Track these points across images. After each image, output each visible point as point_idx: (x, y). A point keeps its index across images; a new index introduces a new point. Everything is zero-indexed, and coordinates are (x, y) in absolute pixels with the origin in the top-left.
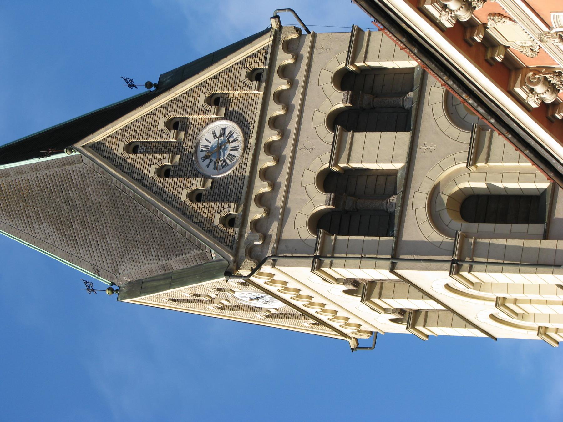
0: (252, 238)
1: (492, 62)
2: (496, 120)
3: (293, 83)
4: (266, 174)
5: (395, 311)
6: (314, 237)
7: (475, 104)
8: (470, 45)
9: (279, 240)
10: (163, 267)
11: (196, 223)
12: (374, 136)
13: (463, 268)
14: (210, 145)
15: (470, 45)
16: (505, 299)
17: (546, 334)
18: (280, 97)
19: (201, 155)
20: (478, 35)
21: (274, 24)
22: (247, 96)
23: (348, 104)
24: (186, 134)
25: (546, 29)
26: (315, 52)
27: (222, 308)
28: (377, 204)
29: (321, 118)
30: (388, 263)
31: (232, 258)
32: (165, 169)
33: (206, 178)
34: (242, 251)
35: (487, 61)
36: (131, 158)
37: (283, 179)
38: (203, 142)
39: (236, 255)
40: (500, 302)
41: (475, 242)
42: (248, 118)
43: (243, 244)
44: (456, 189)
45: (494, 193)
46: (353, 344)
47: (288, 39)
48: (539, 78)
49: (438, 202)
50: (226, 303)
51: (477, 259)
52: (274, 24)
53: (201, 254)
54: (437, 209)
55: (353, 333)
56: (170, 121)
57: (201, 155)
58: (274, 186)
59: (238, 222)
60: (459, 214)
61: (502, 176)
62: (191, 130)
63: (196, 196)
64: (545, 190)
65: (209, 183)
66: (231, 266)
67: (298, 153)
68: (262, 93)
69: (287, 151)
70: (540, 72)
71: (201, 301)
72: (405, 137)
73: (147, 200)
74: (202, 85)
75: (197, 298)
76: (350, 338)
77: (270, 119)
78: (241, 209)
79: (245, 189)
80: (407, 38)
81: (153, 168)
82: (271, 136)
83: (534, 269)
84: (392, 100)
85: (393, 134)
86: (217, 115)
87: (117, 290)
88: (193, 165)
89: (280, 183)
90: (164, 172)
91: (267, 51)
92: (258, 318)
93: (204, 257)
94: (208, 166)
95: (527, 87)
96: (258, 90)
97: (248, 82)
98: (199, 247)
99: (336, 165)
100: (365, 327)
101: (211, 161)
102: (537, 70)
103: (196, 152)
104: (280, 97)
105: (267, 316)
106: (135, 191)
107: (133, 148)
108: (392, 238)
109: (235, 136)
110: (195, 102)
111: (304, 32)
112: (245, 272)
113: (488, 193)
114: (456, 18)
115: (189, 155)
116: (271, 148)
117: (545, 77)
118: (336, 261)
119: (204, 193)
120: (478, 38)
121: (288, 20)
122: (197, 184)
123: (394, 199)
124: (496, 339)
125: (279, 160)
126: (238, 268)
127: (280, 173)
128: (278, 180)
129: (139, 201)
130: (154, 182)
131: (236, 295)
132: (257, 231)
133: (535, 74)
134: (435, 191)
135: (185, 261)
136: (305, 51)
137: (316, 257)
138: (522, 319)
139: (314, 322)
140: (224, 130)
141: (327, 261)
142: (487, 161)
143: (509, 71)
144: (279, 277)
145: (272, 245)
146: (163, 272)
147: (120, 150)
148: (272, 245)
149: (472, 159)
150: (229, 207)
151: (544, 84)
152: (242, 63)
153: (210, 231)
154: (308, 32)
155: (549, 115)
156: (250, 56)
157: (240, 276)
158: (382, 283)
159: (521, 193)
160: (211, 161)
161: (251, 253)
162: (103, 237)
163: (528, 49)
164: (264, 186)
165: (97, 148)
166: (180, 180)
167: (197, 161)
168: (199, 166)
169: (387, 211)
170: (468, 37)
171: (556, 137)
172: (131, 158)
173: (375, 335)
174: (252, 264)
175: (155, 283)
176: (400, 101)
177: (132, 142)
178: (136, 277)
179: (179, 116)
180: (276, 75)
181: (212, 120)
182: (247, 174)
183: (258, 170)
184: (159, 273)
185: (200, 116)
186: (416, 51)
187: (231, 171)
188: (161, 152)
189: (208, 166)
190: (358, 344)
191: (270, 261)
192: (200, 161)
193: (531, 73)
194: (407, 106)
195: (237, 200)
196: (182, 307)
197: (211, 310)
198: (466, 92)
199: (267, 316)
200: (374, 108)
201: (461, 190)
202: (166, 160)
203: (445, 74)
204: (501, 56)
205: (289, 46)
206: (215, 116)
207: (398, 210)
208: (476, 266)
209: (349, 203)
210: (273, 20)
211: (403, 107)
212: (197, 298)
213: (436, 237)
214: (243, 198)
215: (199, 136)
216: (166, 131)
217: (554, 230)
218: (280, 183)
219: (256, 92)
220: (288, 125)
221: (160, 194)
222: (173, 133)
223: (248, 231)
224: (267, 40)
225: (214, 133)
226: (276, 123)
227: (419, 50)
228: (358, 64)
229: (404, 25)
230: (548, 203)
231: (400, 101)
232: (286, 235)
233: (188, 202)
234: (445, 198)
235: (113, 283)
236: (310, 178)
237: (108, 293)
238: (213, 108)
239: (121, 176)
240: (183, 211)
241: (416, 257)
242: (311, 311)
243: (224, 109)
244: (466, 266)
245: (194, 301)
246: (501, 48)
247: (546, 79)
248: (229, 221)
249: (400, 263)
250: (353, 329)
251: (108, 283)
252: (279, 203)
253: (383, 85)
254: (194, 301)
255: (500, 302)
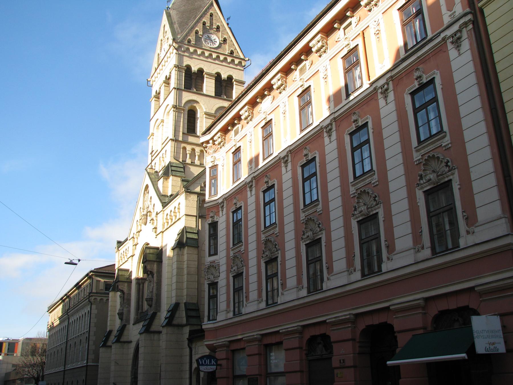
0: (184, 48)
1: (257, 98)
2: (236, 101)
3: (229, 63)
4: (203, 53)
5: (160, 92)
6: (184, 66)
7: (242, 94)
8: (264, 90)
9: (183, 55)
10: (175, 22)
11: (189, 32)
12: (213, 85)
13: (174, 109)
14: (212, 38)
15: (264, 90)
16: (164, 122)
17: (152, 135)
18: (225, 59)
19: (209, 35)
20: (231, 128)
21: (247, 59)
22: (226, 50)
23: (223, 79)
24: (215, 31)
25: (268, 114)
26: (238, 70)
27: (161, 40)
28: (193, 85)
29: (219, 71)
30: (176, 87)
31: (178, 41)
32: (205, 24)
33: (202, 36)
34: (180, 44)
35: (258, 96)
36: (209, 14)
37: (201, 58)
38: (213, 36)
39: (179, 42)
40: (163, 121)
41: (182, 113)
42: (219, 49)
43: (182, 45)
44: (197, 108)
45: (196, 119)
46: (149, 80)
47: (242, 63)
48: (250, 113)
49: (194, 103)
50: (163, 42)
51: (177, 113)
52: (247, 59)
53: (179, 33)
54: (191, 102)
55: (153, 80)
56: (219, 27)
57: (209, 35)
58: (199, 55)
59: (189, 44)
60: (190, 109)
61: (201, 122)
62: (216, 32)
63: (197, 32)
64: (196, 134)
65: (201, 36)
66: (176, 41)
67: (209, 63)
68: (227, 54)
69: (209, 60)
70: (252, 114)
71: (164, 34)
72: (213, 95)
73: (196, 18)
74: (230, 37)
75: (165, 33)
76: (151, 79)
77: (219, 56)
78: (193, 45)
79: (199, 47)
80: (268, 69)
81: (206, 21)
82: (214, 56)
83: (174, 129)
84: (224, 92)
85: (214, 91)
86: (221, 40)
87: (168, 9)
88: (206, 32)
89: (200, 57)
90: (204, 24)
91: (239, 56)
92: (158, 51)
93: (178, 33)
94: (206, 37)
95: (247, 110)
96: (228, 53)
97: (230, 50)
98: (181, 32)
99: (205, 74)
100: (154, 83)
101: (207, 38)
102: (252, 113)
103: (210, 33)
104: (225, 59)
105: (158, 54)
106: (199, 15)
107: (211, 15)
108: (183, 89)
109: (214, 45)
110: (225, 34)
111: (244, 68)
112: (174, 44)
113: (196, 118)
114: (275, 84)
115: (209, 31)
116: (211, 55)
117: (284, 84)
118: (177, 72)
119: (198, 35)
120: (236, 122)
121: (248, 63)
122: (201, 33)
123: (195, 90)
124: (150, 121)
125: (207, 57)
126: (175, 43)
127: (203, 57)
128: (201, 57)
129: (196, 16)
130: (201, 20)
131: (166, 44)
132: (186, 49)
133: (224, 138)
134: (197, 102)
135: (177, 29)
136: (238, 67)
137: (178, 66)
138: (157, 128)
139: (156, 68)
140: (216, 42)
141: (177, 69)
142: (206, 118)
143: (225, 131)
144: (172, 55)
145: (182, 53)
146: (173, 22)
147: (211, 11)
148: (182, 53)
149: (207, 114)
150: (194, 42)
151: (221, 141)
152: (236, 49)
153: (187, 35)
154: (244, 69)
155: (304, 53)
156: (237, 52)
157: (173, 43)
158: (168, 87)
159: (196, 127)
160: (207, 38)
161: (180, 47)
162: (184, 6)
163: (295, 77)
164: (200, 52)
165: (212, 4)
166: (202, 28)
167: (207, 34)
168: (206, 34)
169: (191, 88)
170: (266, 89)
171: (291, 60)
172: (209, 14)
173: (152, 86)
174: (176, 47)
175: (170, 20)
176: (223, 94)
177: (213, 15)
178: (172, 15)
179: (221, 29)
180: (232, 58)
181: (219, 39)
182: (203, 48)
183: (204, 51)
184: (173, 21)
185: (220, 36)
186: (264, 72)
187: (204, 43)
188: (210, 23)
189: (206, 37)
190: (149, 81)
191: (177, 52)
192: (207, 34)
193: (252, 111)
194: (222, 96)
195: (195, 44)
196: (162, 28)
197: (161, 36)
198: (247, 90)
199: (158, 54)
200: (221, 86)
201: (197, 110)
202: (208, 24)
203: (254, 83)
204: (337, 26)
205: (240, 63)
206: (220, 40)
207: (192, 91)
208: (175, 112)
209: (194, 77)
210: (248, 59)
211: (221, 95)
212: (165, 33)
213: (184, 102)
214: (196, 46)
215: (215, 35)
216: (216, 25)
217: (185, 136)
218: (200, 57)
219: (227, 52)
220: (217, 61)
221: (198, 22)
222: (216, 27)
223: (186, 46)
224: (242, 57)
225: (215, 39)
226: (218, 57)
227: (264, 73)
228: (234, 83)
229: (274, 67)
230: (193, 135)
231: (223, 94)
232: (185, 58)
233: (195, 30)
234: (195, 105)
235: (170, 8)
236: (202, 66)
237: (167, 7)
238: (223, 40)
239: (203, 11)
240: (193, 28)
241: (178, 95)
242: (160, 67)
243: (222, 43)
244: (175, 110)
245: (164, 32)
246: (340, 26)
247: (250, 116)
248: (189, 41)
249: (176, 90)
250: (154, 80)
251: (170, 7)
252: (194, 56)
253: (228, 89)
254: (164, 32)
255: (163, 121)
